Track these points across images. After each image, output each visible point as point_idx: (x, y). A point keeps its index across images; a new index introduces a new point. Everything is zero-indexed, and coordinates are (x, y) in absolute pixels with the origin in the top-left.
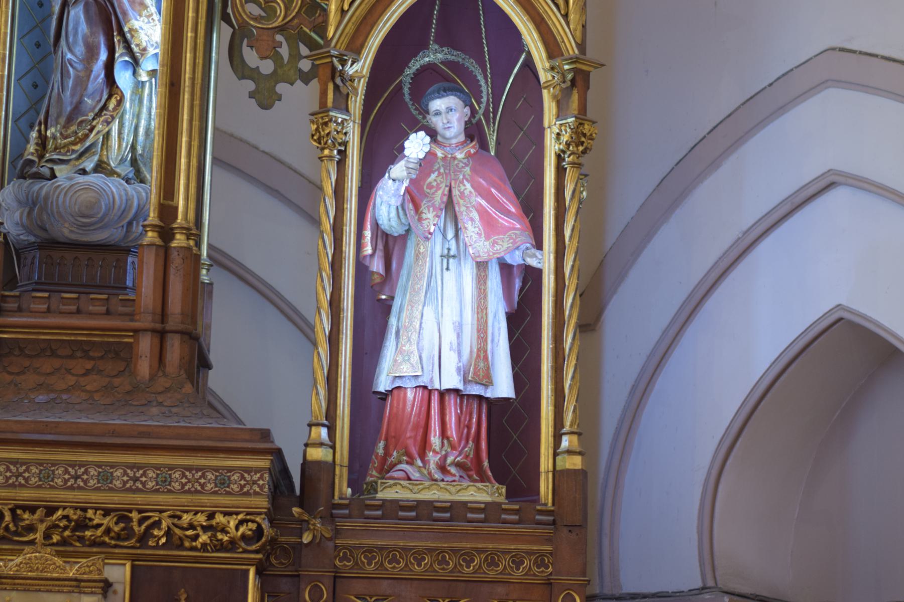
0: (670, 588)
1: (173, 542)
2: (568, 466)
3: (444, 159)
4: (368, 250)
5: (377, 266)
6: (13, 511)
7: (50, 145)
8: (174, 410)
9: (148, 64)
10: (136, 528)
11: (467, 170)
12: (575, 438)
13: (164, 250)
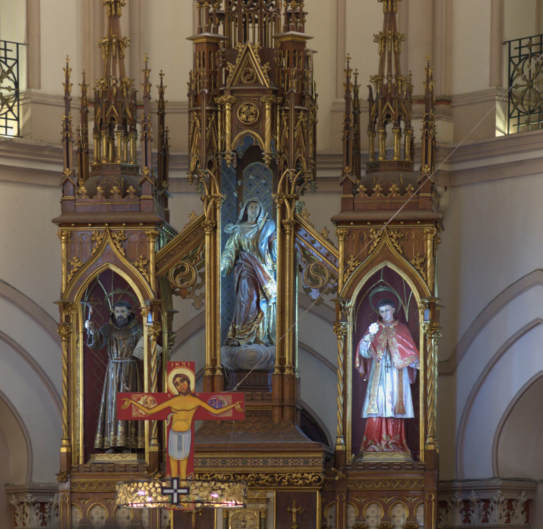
0: (482, 477)
1: (290, 483)
2: (429, 449)
3: (385, 329)
4: (358, 365)
5: (361, 371)
6: (234, 475)
7: (237, 332)
8: (288, 435)
9: (272, 301)
10: (277, 480)
11: (394, 333)
12: (431, 438)
13: (282, 376)
